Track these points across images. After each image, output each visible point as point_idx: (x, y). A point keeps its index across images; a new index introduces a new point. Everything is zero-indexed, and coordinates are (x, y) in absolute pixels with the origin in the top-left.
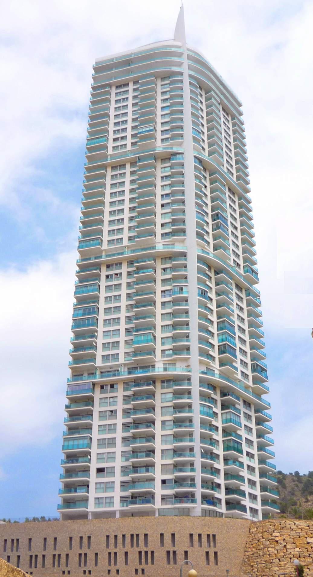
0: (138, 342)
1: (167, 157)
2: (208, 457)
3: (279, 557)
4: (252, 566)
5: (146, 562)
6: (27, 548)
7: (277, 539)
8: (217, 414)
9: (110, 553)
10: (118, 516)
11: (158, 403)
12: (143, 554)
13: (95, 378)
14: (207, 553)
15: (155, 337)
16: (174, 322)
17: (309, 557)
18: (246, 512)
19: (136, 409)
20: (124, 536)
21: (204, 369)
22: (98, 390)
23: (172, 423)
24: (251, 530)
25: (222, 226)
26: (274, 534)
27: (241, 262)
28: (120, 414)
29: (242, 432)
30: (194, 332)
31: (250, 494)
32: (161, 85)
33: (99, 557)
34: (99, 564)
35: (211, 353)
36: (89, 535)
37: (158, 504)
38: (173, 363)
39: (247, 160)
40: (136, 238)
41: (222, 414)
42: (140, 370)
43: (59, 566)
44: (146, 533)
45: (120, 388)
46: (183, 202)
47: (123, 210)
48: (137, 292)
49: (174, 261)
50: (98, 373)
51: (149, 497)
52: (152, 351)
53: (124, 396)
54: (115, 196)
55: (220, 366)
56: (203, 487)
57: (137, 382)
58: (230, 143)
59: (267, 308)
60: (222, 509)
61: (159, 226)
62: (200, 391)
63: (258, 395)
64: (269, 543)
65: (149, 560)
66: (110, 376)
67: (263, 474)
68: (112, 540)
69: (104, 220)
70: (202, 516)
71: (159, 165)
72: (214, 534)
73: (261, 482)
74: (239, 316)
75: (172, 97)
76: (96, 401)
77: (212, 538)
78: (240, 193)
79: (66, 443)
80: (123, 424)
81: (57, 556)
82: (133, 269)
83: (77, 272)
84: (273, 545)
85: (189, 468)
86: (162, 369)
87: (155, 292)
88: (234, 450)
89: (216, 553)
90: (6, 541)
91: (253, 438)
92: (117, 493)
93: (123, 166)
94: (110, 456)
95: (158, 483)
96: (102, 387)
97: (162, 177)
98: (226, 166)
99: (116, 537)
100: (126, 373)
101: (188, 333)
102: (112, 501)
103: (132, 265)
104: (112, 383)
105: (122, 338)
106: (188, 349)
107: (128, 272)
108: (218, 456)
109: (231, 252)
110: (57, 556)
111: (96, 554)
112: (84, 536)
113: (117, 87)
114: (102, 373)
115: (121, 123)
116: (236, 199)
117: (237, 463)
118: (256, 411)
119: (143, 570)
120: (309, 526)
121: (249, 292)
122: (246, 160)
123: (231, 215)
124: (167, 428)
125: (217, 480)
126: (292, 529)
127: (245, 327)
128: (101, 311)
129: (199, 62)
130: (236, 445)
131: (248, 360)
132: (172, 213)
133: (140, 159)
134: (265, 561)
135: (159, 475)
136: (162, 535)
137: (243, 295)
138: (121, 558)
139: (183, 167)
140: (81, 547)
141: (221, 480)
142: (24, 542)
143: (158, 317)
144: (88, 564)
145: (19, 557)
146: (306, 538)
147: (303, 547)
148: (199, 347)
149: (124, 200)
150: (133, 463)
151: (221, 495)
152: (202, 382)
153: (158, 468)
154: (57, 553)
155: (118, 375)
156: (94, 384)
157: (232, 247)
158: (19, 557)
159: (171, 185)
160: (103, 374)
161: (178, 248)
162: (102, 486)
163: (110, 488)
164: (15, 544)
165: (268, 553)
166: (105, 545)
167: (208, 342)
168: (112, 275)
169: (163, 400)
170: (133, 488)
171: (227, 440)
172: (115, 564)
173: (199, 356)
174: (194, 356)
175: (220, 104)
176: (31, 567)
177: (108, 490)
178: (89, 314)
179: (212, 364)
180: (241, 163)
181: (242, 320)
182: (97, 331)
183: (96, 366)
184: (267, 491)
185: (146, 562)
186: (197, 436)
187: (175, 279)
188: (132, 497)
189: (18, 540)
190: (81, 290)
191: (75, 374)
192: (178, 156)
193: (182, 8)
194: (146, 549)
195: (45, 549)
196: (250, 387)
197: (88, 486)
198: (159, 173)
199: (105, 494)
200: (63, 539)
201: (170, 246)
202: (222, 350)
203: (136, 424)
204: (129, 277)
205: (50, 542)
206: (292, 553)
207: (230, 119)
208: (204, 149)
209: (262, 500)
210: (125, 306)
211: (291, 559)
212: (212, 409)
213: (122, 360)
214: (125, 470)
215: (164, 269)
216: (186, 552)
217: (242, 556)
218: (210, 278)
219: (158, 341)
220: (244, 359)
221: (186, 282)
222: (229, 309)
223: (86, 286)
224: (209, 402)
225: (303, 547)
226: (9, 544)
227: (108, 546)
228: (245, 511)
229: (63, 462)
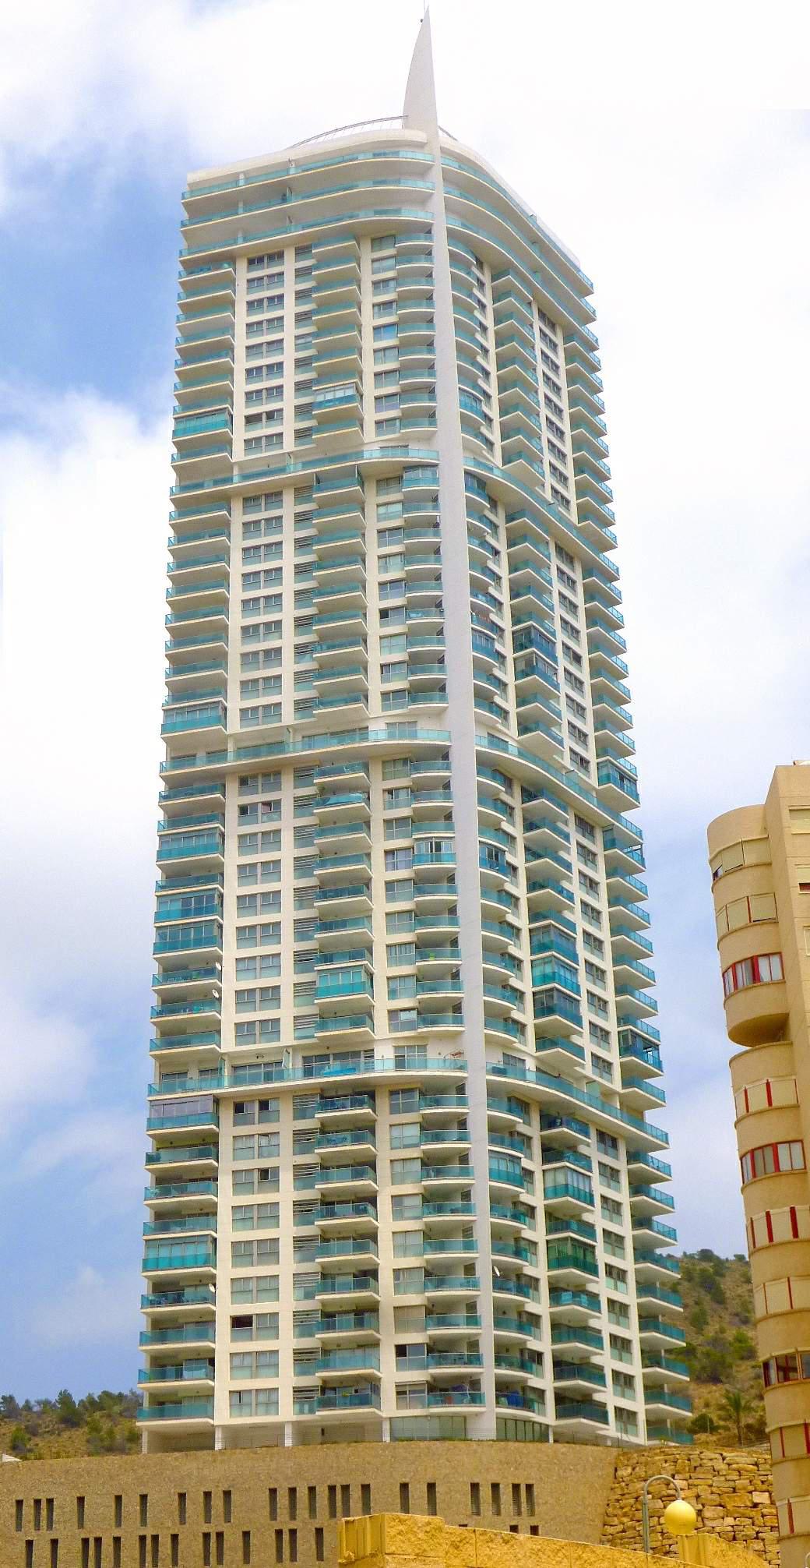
0: (328, 992)
1: (390, 478)
8: (530, 1173)
9: (279, 1533)
11: (383, 1151)
15: (371, 976)
16: (419, 936)
18: (606, 1422)
20: (312, 1490)
21: (497, 1060)
22: (227, 1114)
23: (418, 1201)
24: (619, 1473)
25: (540, 665)
27: (590, 754)
28: (286, 1178)
29: (596, 1217)
30: (472, 964)
31: (614, 1338)
33: (253, 1540)
34: (254, 1558)
35: (516, 1015)
36: (226, 1488)
37: (389, 1406)
39: (589, 292)
40: (317, 707)
42: (334, 1064)
47: (280, 365)
49: (417, 769)
50: (226, 1072)
51: (365, 1390)
52: (363, 1016)
53: (296, 1133)
54: (260, 332)
55: (538, 1049)
57: (328, 1097)
60: (548, 1415)
61: (374, 671)
62: (485, 970)
63: (635, 1113)
66: (254, 1080)
67: (644, 1252)
68: (283, 1500)
70: (498, 1440)
71: (367, 254)
72: (530, 1482)
73: (642, 1341)
74: (574, 727)
75: (403, 300)
76: (225, 1145)
78: (588, 559)
79: (153, 1254)
80: (296, 702)
81: (149, 1541)
85: (463, 1314)
86: (391, 1064)
87: (368, 855)
88: (576, 1266)
90: (19, 1503)
91: (625, 1228)
92: (286, 1379)
93: (277, 256)
94: (264, 1285)
96: (239, 1108)
98: (551, 482)
100: (300, 1073)
103: (307, 523)
104: (263, 1098)
105: (287, 978)
106: (457, 1008)
108: (534, 1282)
109: (547, 468)
111: (246, 1534)
114: (235, 1068)
116: (558, 339)
117: (584, 1298)
118: (633, 1156)
120: (756, 1464)
121: (570, 335)
123: (547, 379)
125: (533, 1344)
126: (716, 1472)
127: (604, 933)
129: (474, 187)
131: (611, 1025)
132: (412, 636)
136: (404, 1487)
139: (433, 398)
140: (208, 1520)
141: (542, 1343)
142: (65, 1507)
143: (379, 921)
145: (54, 1542)
149: (281, 318)
150: (324, 1303)
151: (545, 1380)
154: (149, 1532)
155: (281, 1078)
156: (217, 1100)
157: (548, 457)
158: (54, 1542)
159: (407, 556)
160: (240, 1072)
161: (427, 736)
162: (248, 1361)
163: (269, 1366)
164: (44, 1513)
165: (659, 1528)
166: (266, 1511)
167: (499, 830)
169: (396, 1143)
170: (326, 1366)
171: (558, 1240)
173: (486, 1026)
175: (531, 288)
178: (199, 912)
179: (518, 1045)
180: (591, 469)
181: (580, 710)
182: (219, 959)
183: (222, 1051)
184: (659, 1365)
186: (481, 1199)
188: (324, 1390)
189: (50, 1501)
190: (175, 845)
191: (164, 1072)
195: (119, 1524)
196: (613, 1093)
197: (212, 1362)
199: (255, 1385)
200: (162, 1501)
201: (399, 451)
202: (543, 1007)
203: (329, 1204)
205: (131, 1506)
206: (718, 1529)
209: (640, 1317)
213: (288, 1036)
215: (390, 792)
218: (509, 810)
219: (381, 986)
220: (597, 991)
221: (450, 828)
222: (560, 893)
226: (28, 1510)
227: (273, 1515)
228: (603, 1418)
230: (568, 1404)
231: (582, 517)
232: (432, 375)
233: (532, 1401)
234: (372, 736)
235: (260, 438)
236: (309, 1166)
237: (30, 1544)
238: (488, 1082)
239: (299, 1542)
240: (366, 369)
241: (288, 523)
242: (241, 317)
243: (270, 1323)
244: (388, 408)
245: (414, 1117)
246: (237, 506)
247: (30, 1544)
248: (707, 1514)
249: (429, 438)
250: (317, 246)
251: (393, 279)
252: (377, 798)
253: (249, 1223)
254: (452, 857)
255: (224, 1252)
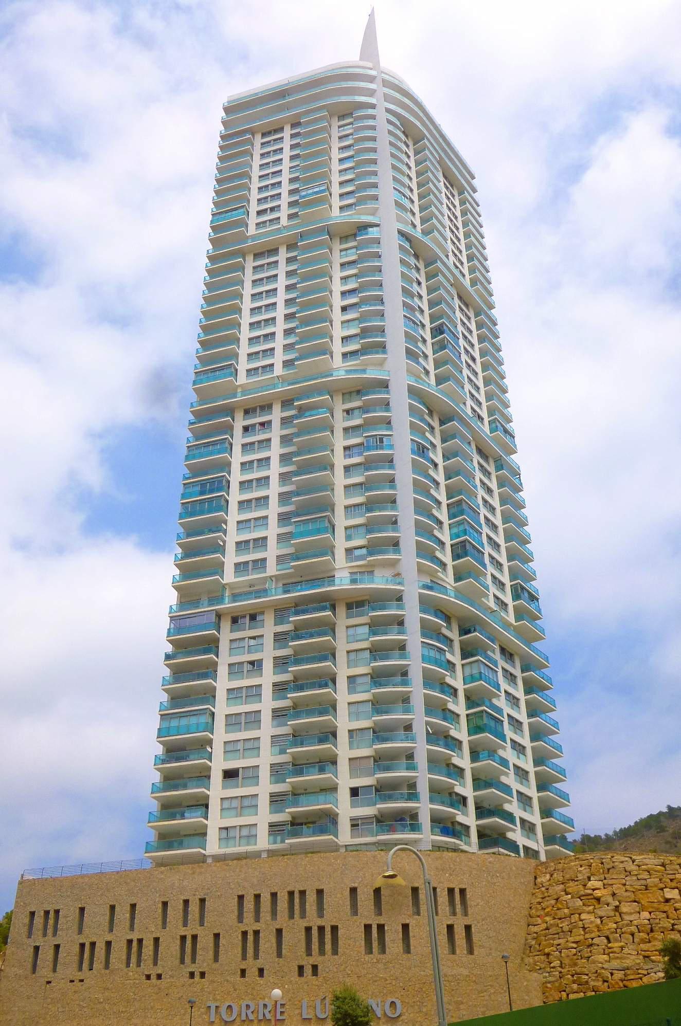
2: (441, 743)
3: (608, 933)
4: (548, 955)
5: (322, 952)
6: (75, 927)
7: (598, 893)
9: (245, 934)
10: (264, 855)
11: (342, 645)
12: (315, 932)
13: (222, 603)
14: (450, 928)
17: (673, 930)
19: (297, 658)
20: (274, 895)
22: (226, 625)
24: (539, 880)
25: (450, 346)
26: (590, 884)
28: (268, 666)
30: (407, 515)
32: (339, 127)
33: (222, 941)
34: (222, 957)
37: (345, 836)
38: (369, 571)
40: (296, 456)
41: (463, 665)
43: (139, 965)
44: (320, 888)
45: (269, 619)
46: (381, 300)
48: (296, 629)
51: (325, 821)
53: (276, 635)
56: (432, 801)
57: (299, 606)
59: (531, 492)
61: (337, 342)
64: (581, 903)
65: (328, 946)
68: (249, 904)
71: (337, 246)
76: (224, 646)
77: (458, 897)
80: (275, 685)
81: (135, 944)
82: (292, 412)
84: (591, 908)
86: (348, 581)
89: (468, 928)
90: (32, 914)
92: (264, 817)
94: (249, 745)
95: (344, 795)
96: (235, 620)
97: (342, 265)
99: (257, 897)
100: (280, 590)
101: (396, 516)
102: (253, 833)
104: (252, 612)
107: (282, 419)
110: (135, 944)
111: (217, 936)
112: (191, 899)
119: (315, 968)
120: (663, 865)
121: (500, 464)
124: (359, 689)
126: (629, 873)
130: (492, 723)
133: (302, 235)
134: (576, 942)
135: (345, 780)
136: (353, 891)
137: (491, 468)
138: (268, 942)
140: (185, 924)
141: (466, 789)
144: (198, 958)
145: (57, 947)
146: (662, 889)
147: (658, 910)
148: (417, 541)
151: (469, 818)
152: (426, 604)
153: (343, 766)
154: (135, 936)
156: (219, 616)
162: (235, 803)
164: (51, 922)
168: (254, 425)
170: (296, 805)
171: (475, 713)
172: (256, 956)
174: (408, 558)
176: (80, 969)
177: (246, 811)
178: (211, 491)
185: (322, 952)
187: (368, 424)
189: (57, 912)
191: (183, 600)
193: (371, 16)
194: (320, 922)
195: (111, 930)
196: (512, 625)
197: (207, 806)
199: (239, 821)
200: (148, 906)
203: (299, 683)
205: (123, 914)
210: (278, 476)
211: (633, 935)
212: (445, 655)
213: (272, 569)
214: (277, 772)
216: (405, 927)
217: (524, 934)
219: (340, 532)
221: (391, 429)
224: (439, 642)
225: (658, 910)
226: (39, 920)
227: (240, 918)
229: (158, 761)
230: (489, 838)
232: (392, 467)
233: (460, 832)
236: (286, 657)
237: (37, 949)
239: (261, 942)
240: (336, 205)
242: (257, 161)
243: (252, 774)
245: (364, 619)
247: (37, 949)
248: (624, 908)
249: (381, 363)
252: (339, 414)
254: (391, 447)
255: (220, 722)
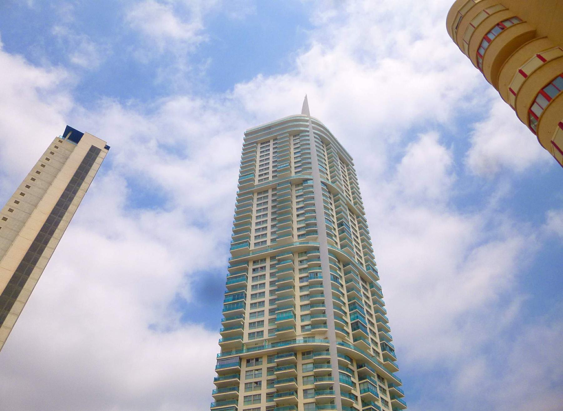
0: (280, 319)
1: (304, 251)
11: (300, 374)
15: (295, 315)
19: (279, 380)
22: (244, 363)
23: (313, 391)
28: (264, 384)
30: (330, 310)
38: (312, 336)
41: (360, 384)
47: (266, 227)
48: (278, 366)
53: (268, 368)
54: (261, 212)
55: (354, 342)
57: (279, 354)
58: (355, 225)
69: (251, 235)
71: (294, 189)
76: (243, 374)
80: (267, 394)
83: (229, 268)
86: (302, 341)
93: (264, 260)
96: (248, 361)
101: (324, 310)
107: (271, 273)
113: (262, 144)
115: (257, 305)
121: (372, 285)
122: (371, 245)
128: (249, 296)
137: (368, 287)
149: (264, 302)
156: (241, 359)
168: (257, 268)
178: (238, 299)
192: (309, 181)
193: (306, 97)
198: (294, 194)
204: (270, 324)
207: (355, 217)
208: (337, 243)
213: (266, 336)
219: (298, 318)
221: (321, 269)
223: (236, 277)
231: (385, 359)
234: (297, 342)
235: (255, 322)
238: (337, 347)
241: (268, 268)
244: (300, 224)
246: (251, 264)
250: (278, 256)
251: (306, 260)
253: (249, 402)
